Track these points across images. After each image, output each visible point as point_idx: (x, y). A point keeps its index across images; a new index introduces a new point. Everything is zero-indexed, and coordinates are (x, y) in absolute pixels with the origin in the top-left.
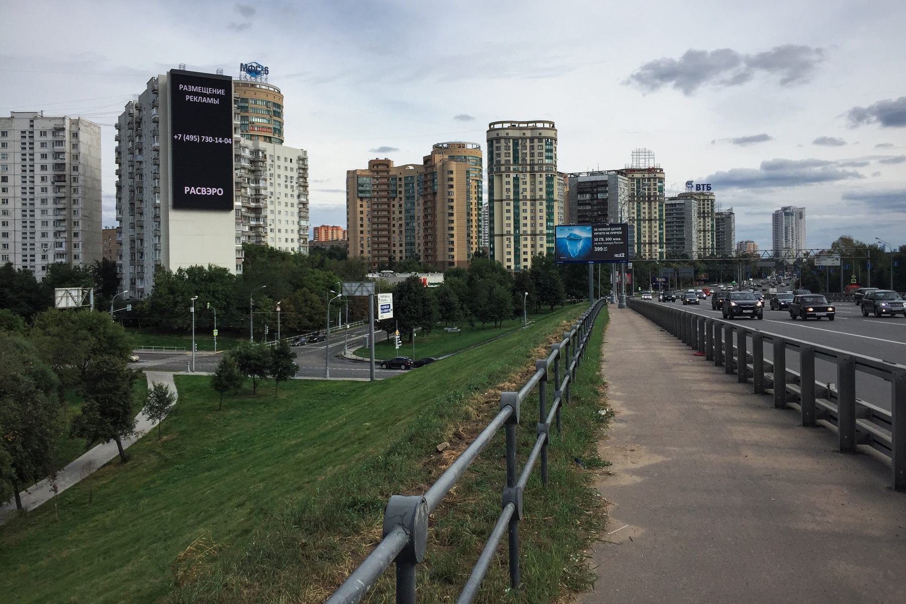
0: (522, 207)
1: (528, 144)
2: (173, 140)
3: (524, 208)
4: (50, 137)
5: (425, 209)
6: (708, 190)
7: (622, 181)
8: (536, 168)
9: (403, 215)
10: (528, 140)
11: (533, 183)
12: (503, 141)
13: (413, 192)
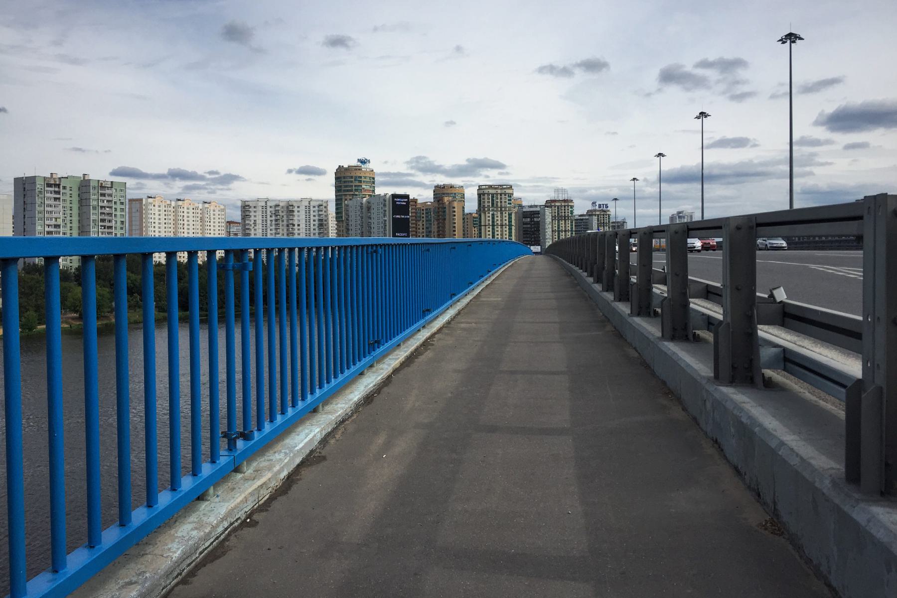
0: (496, 229)
1: (499, 197)
2: (393, 218)
3: (497, 229)
4: (317, 208)
5: (438, 227)
6: (606, 208)
7: (548, 211)
8: (503, 209)
9: (424, 231)
10: (499, 195)
11: (502, 217)
12: (486, 195)
13: (431, 217)
